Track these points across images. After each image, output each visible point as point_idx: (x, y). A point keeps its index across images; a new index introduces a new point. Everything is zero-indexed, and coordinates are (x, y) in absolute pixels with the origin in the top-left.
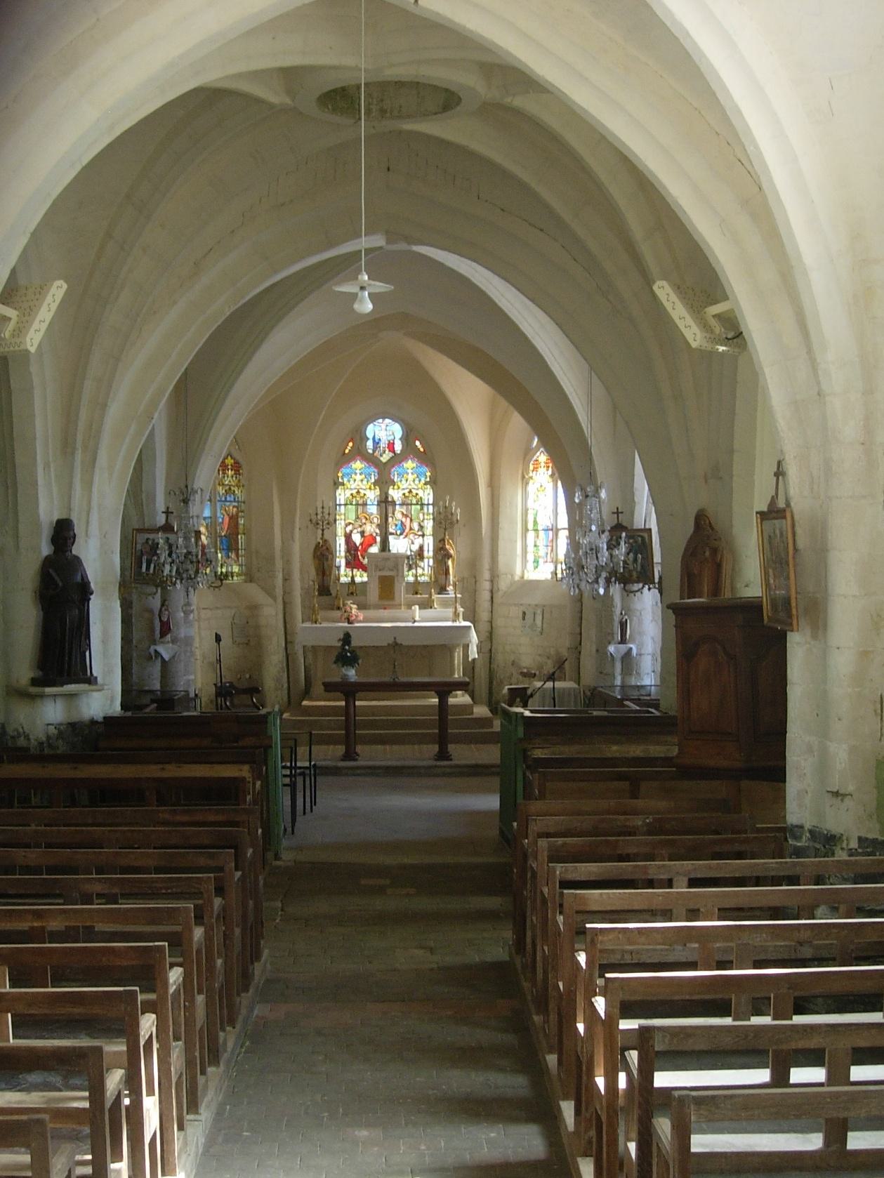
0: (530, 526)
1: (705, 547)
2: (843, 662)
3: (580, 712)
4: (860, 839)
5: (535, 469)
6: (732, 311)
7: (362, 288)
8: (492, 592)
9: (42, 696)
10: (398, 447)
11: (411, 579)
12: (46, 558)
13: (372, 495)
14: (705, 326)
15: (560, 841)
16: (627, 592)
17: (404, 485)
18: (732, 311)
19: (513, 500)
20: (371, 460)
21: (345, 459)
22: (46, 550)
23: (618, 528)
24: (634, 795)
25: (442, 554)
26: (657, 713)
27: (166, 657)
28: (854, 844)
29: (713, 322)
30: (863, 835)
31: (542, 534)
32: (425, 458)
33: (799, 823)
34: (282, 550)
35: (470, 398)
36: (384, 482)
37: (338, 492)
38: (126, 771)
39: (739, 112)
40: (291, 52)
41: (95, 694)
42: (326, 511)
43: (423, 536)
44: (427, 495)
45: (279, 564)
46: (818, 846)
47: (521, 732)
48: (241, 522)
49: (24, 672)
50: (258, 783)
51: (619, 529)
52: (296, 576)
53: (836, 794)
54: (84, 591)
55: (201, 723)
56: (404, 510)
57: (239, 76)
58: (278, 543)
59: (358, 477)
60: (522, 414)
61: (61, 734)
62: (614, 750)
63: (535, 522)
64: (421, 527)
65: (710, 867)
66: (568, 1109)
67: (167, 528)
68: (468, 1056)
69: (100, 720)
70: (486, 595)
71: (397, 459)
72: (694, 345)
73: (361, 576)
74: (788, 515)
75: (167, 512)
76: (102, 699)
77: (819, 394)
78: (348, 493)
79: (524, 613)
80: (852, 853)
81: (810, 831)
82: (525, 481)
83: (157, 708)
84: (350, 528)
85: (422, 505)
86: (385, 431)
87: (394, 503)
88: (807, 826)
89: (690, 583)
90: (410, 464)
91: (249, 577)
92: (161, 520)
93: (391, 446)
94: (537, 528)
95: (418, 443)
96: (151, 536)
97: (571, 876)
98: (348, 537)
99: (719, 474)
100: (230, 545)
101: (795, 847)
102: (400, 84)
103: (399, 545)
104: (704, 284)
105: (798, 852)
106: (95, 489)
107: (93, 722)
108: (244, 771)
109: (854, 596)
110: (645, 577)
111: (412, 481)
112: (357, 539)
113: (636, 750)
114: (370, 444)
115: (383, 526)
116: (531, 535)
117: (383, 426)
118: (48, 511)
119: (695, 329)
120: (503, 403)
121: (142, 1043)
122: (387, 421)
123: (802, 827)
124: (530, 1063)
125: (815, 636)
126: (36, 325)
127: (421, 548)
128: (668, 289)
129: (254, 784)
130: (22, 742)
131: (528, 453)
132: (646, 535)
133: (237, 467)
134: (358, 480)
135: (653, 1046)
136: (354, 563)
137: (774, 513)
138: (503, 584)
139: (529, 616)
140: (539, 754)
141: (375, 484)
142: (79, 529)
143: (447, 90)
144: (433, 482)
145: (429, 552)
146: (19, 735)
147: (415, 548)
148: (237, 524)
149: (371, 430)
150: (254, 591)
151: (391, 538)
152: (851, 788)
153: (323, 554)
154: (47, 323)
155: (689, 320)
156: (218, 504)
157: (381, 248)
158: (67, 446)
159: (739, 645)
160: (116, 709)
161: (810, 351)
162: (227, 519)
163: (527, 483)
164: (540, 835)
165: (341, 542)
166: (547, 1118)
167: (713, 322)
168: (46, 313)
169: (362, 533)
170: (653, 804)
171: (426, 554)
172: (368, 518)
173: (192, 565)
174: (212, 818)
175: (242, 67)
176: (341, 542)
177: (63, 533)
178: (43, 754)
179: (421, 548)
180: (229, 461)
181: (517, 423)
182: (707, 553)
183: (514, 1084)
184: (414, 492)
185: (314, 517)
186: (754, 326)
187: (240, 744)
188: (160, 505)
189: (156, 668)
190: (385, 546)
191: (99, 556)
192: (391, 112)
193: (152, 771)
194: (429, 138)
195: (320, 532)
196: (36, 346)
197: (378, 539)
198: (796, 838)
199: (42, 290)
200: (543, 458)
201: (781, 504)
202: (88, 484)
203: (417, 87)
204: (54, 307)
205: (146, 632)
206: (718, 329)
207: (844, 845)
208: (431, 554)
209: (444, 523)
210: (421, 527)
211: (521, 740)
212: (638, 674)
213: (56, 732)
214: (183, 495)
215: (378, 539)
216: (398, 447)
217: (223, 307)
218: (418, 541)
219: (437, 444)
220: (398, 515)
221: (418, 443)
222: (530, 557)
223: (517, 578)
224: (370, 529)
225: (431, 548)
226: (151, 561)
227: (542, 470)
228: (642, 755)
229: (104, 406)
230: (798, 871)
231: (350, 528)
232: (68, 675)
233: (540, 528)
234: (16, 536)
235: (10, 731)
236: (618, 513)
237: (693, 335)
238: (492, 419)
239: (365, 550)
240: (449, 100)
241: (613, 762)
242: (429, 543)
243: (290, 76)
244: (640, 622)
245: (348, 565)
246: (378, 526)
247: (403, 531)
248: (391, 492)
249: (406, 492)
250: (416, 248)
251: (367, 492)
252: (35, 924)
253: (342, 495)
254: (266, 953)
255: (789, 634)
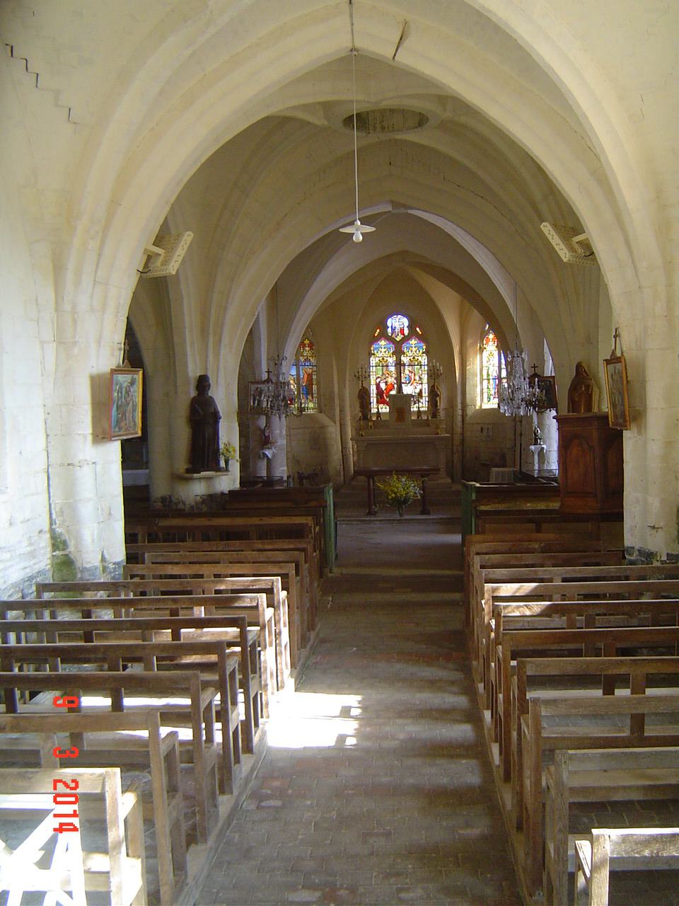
0: (485, 377)
1: (582, 381)
2: (655, 448)
3: (513, 484)
4: (668, 554)
5: (487, 343)
6: (587, 239)
7: (357, 230)
8: (463, 416)
9: (192, 479)
10: (406, 332)
11: (416, 409)
12: (194, 398)
13: (392, 360)
14: (572, 249)
15: (487, 557)
16: (540, 413)
17: (410, 354)
18: (587, 239)
19: (474, 364)
20: (391, 340)
21: (375, 340)
22: (193, 393)
23: (535, 375)
24: (539, 531)
25: (433, 394)
26: (556, 484)
27: (270, 456)
28: (664, 558)
29: (576, 246)
30: (670, 552)
31: (491, 381)
32: (421, 338)
33: (632, 546)
34: (339, 394)
35: (448, 304)
36: (398, 353)
37: (371, 359)
38: (239, 521)
39: (586, 117)
40: (325, 92)
41: (224, 477)
42: (364, 370)
43: (422, 384)
44: (424, 359)
45: (337, 402)
46: (643, 559)
47: (474, 496)
48: (314, 377)
49: (182, 465)
50: (317, 529)
51: (536, 377)
52: (348, 409)
53: (653, 527)
54: (216, 417)
55: (284, 495)
56: (410, 368)
57: (295, 108)
58: (336, 390)
59: (383, 350)
60: (478, 310)
61: (204, 501)
62: (529, 506)
63: (488, 375)
64: (420, 378)
65: (574, 571)
66: (487, 715)
67: (268, 381)
68: (432, 684)
69: (227, 492)
70: (459, 418)
71: (406, 339)
72: (565, 260)
73: (386, 408)
74: (623, 360)
75: (268, 372)
76: (229, 481)
77: (639, 287)
78: (377, 360)
79: (482, 428)
80: (663, 562)
81: (639, 551)
82: (482, 350)
83: (263, 486)
84: (379, 380)
85: (421, 365)
86: (398, 323)
87: (404, 365)
88: (637, 547)
89: (573, 405)
90: (413, 342)
91: (320, 409)
92: (265, 376)
93: (402, 331)
94: (485, 375)
95: (418, 329)
96: (259, 386)
97: (491, 576)
98: (378, 386)
99: (591, 341)
100: (309, 391)
101: (630, 560)
102: (392, 111)
103: (407, 390)
104: (571, 226)
105: (632, 563)
106: (222, 357)
107: (223, 494)
108: (309, 520)
109: (662, 409)
110: (552, 404)
111: (415, 351)
112: (383, 386)
113: (542, 506)
114: (389, 330)
115: (399, 379)
116: (485, 382)
117: (397, 319)
118: (194, 371)
119: (565, 250)
120: (467, 305)
121: (228, 673)
122: (399, 316)
123: (633, 548)
124: (470, 691)
125: (639, 433)
126: (175, 258)
127: (421, 391)
128: (549, 227)
129: (314, 529)
130: (181, 506)
131: (483, 336)
132: (551, 380)
133: (311, 345)
134: (382, 351)
135: (525, 673)
136: (381, 400)
137: (614, 360)
138: (470, 412)
139: (485, 431)
140: (483, 508)
141: (393, 354)
142: (212, 381)
143: (420, 114)
144: (427, 352)
145: (425, 394)
146: (179, 503)
147: (417, 391)
148: (312, 379)
149: (389, 322)
150: (323, 418)
151: (403, 385)
152: (662, 524)
153: (364, 395)
154: (182, 257)
155: (562, 246)
156: (301, 367)
157: (389, 212)
158: (204, 332)
159: (599, 439)
160: (237, 486)
161: (633, 262)
162: (306, 376)
163: (483, 351)
164: (478, 554)
165: (373, 389)
166: (472, 717)
167: (576, 246)
168: (181, 251)
169: (386, 383)
170: (549, 536)
171: (424, 395)
172: (390, 374)
173: (282, 401)
174: (286, 547)
175: (295, 102)
176: (373, 389)
177: (202, 383)
178: (193, 512)
179: (421, 391)
180: (307, 342)
181: (476, 316)
182: (583, 389)
183: (462, 701)
184: (416, 358)
185: (357, 375)
186: (600, 247)
187: (309, 505)
188: (264, 368)
189: (264, 464)
190: (400, 389)
191: (225, 397)
192: (388, 128)
193: (256, 521)
194: (413, 144)
195: (360, 382)
196: (175, 271)
197: (396, 386)
198: (630, 555)
199: (179, 237)
200: (491, 336)
201: (618, 354)
202: (217, 354)
203: (403, 112)
204: (186, 247)
205: (255, 441)
206: (580, 250)
207: (658, 559)
208: (427, 394)
209: (433, 375)
210: (420, 378)
211: (473, 501)
212: (548, 462)
213: (201, 500)
214: (276, 361)
215: (396, 386)
216: (406, 332)
217: (295, 249)
218: (419, 387)
219: (430, 330)
220: (407, 372)
221: (418, 329)
222: (485, 396)
223: (477, 408)
224: (391, 380)
225: (427, 391)
226: (258, 399)
227: (491, 343)
228: (545, 508)
229: (225, 308)
230: (628, 573)
231: (379, 380)
232: (208, 467)
233: (491, 377)
234: (175, 386)
235: (174, 500)
236: (535, 367)
237: (564, 254)
238: (461, 315)
239: (388, 393)
240: (421, 120)
241: (527, 512)
242: (425, 386)
243: (327, 107)
244: (549, 431)
245: (378, 402)
246: (396, 378)
247: (409, 382)
248: (402, 358)
249: (411, 358)
250: (410, 211)
251: (389, 359)
252: (173, 607)
253: (373, 361)
254: (319, 626)
255: (624, 431)
